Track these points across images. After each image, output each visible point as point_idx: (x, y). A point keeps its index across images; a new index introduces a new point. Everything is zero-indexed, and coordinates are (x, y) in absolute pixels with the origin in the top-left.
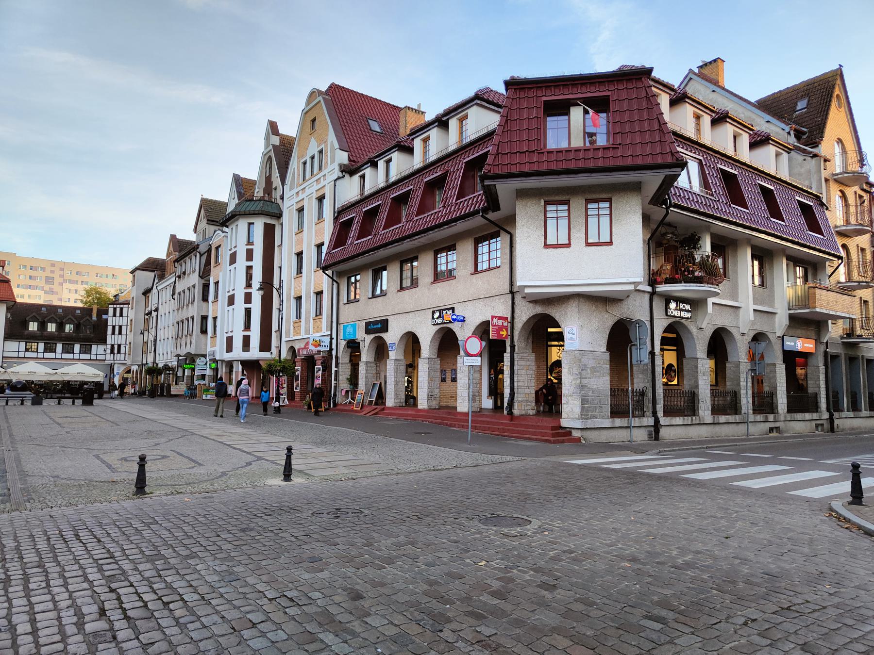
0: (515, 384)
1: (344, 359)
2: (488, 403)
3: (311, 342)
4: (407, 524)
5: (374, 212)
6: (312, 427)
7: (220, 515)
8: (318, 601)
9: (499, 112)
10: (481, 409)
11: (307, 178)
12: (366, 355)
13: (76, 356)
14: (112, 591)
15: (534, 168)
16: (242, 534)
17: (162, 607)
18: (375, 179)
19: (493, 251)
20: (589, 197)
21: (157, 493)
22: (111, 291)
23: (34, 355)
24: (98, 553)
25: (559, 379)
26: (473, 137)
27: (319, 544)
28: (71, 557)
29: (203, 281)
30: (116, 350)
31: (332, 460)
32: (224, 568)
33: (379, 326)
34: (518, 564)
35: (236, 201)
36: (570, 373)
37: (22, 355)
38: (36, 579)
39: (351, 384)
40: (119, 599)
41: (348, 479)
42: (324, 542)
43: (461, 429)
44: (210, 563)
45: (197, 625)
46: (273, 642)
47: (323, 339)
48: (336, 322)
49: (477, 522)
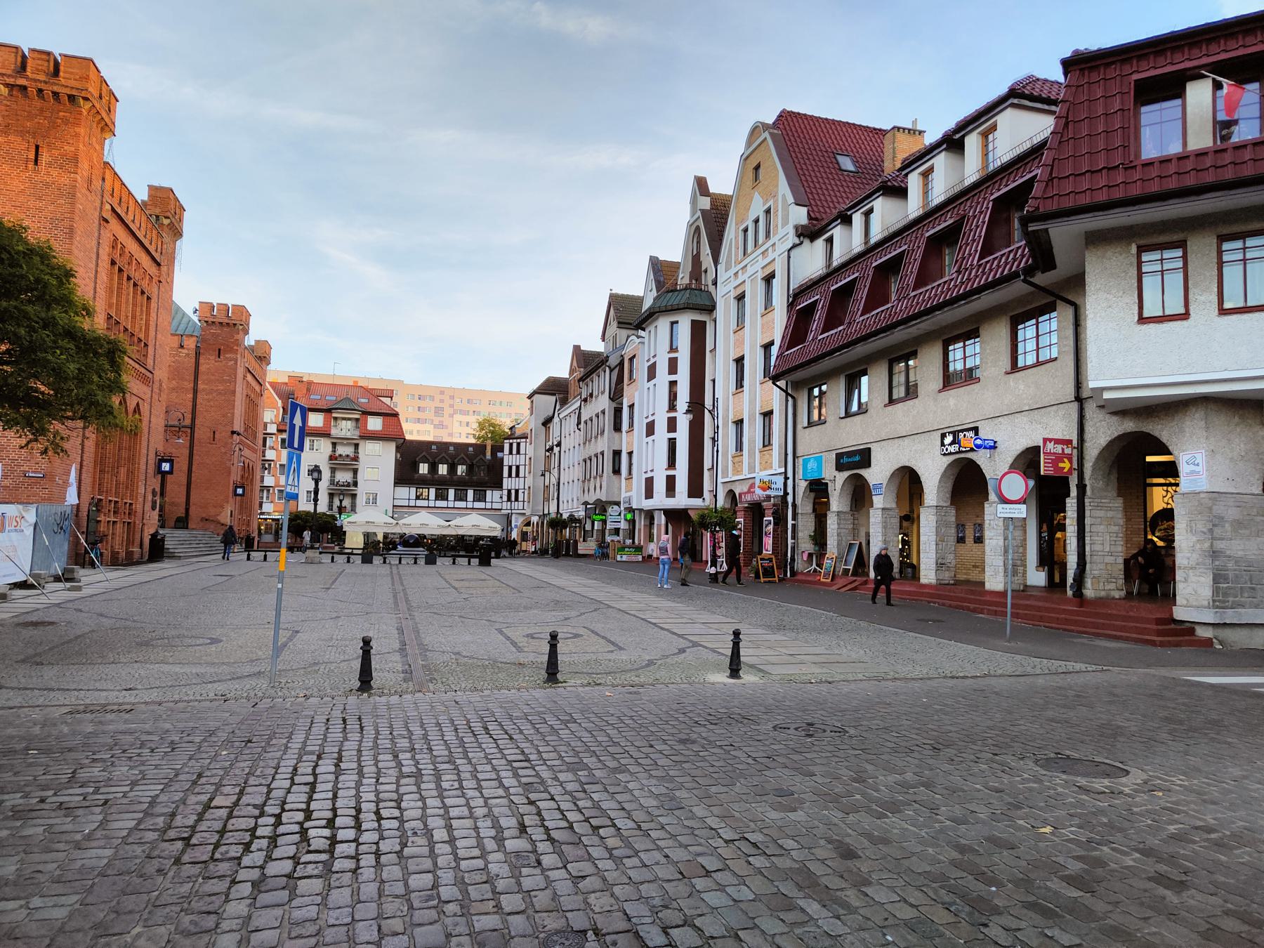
0: (1087, 548)
1: (805, 507)
2: (1037, 578)
3: (758, 483)
4: (916, 755)
5: (848, 289)
6: (762, 603)
7: (651, 718)
8: (793, 853)
9: (1052, 113)
10: (1026, 586)
11: (749, 251)
12: (837, 502)
13: (470, 505)
14: (531, 803)
15: (1118, 194)
16: (682, 747)
17: (590, 832)
18: (848, 241)
19: (1047, 335)
20: (1226, 230)
21: (572, 682)
22: (506, 423)
23: (425, 503)
24: (512, 754)
25: (1169, 539)
26: (1006, 159)
27: (786, 771)
28: (482, 755)
29: (614, 405)
30: (513, 496)
31: (802, 654)
32: (664, 791)
33: (857, 458)
34: (1111, 838)
35: (654, 293)
36: (1191, 530)
37: (412, 503)
38: (448, 777)
39: (815, 544)
40: (539, 814)
41: (821, 682)
42: (795, 769)
43: (991, 618)
44: (644, 782)
45: (635, 861)
46: (734, 900)
47: (774, 479)
48: (792, 455)
49: (1031, 764)
